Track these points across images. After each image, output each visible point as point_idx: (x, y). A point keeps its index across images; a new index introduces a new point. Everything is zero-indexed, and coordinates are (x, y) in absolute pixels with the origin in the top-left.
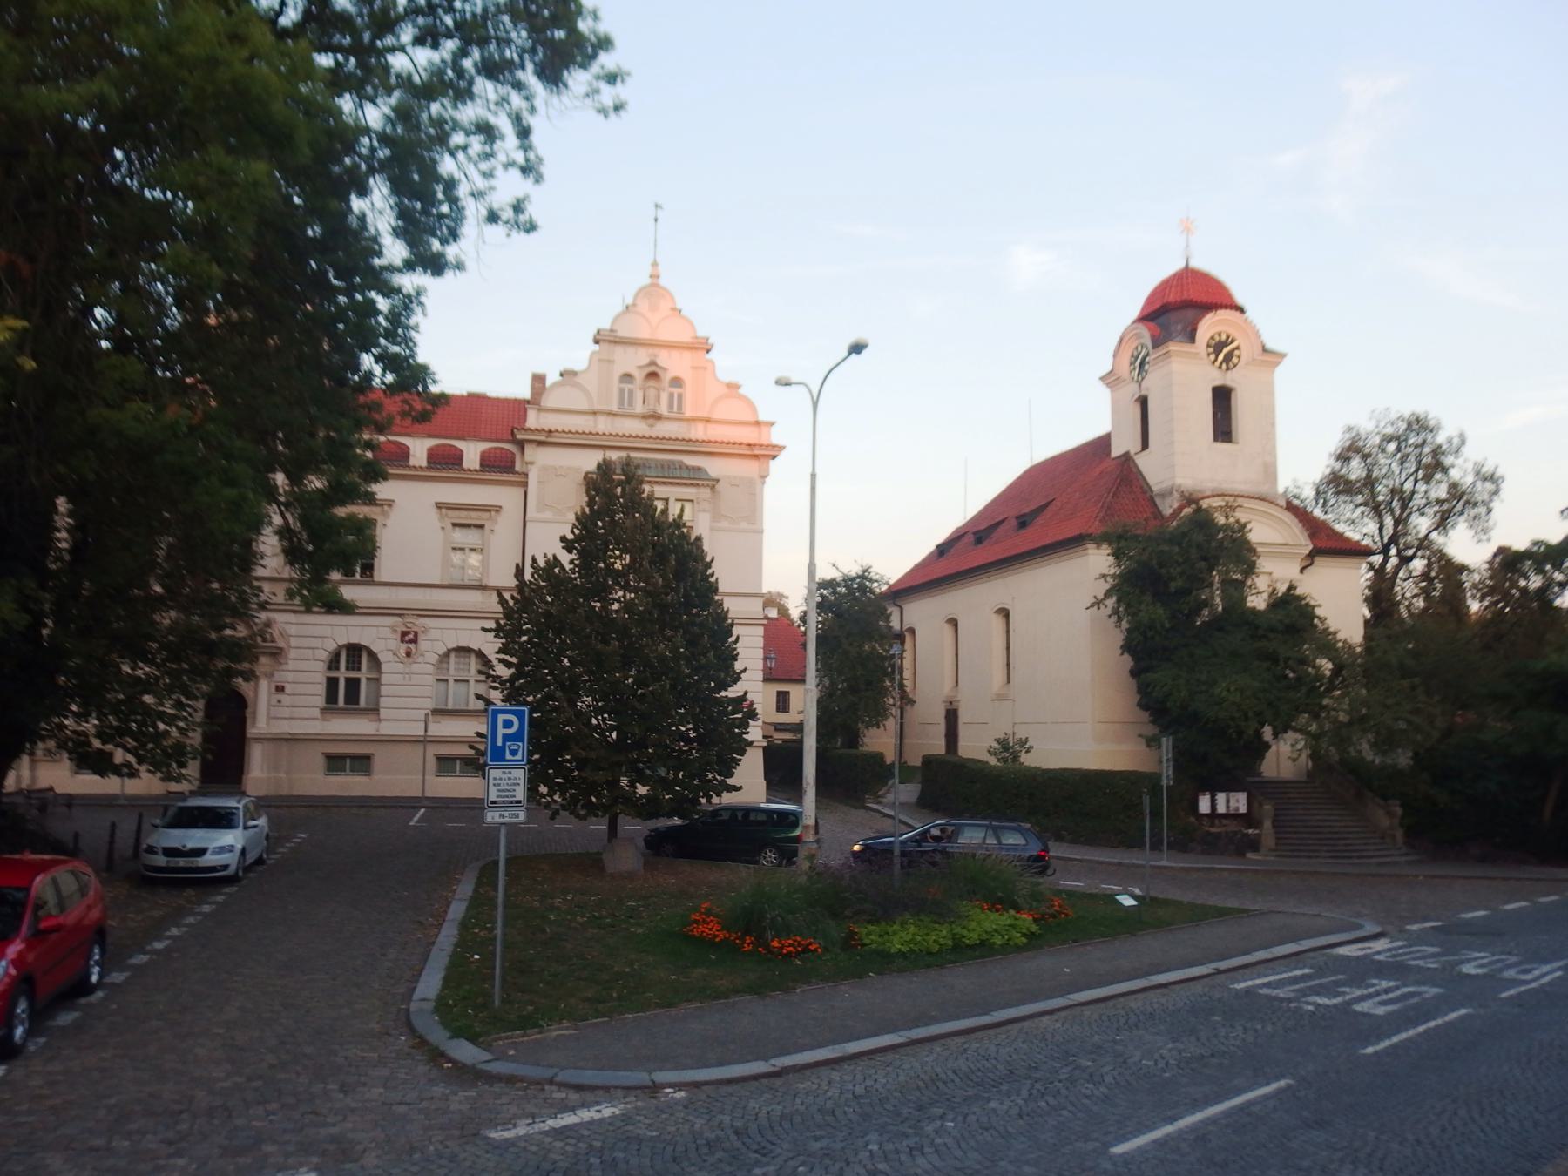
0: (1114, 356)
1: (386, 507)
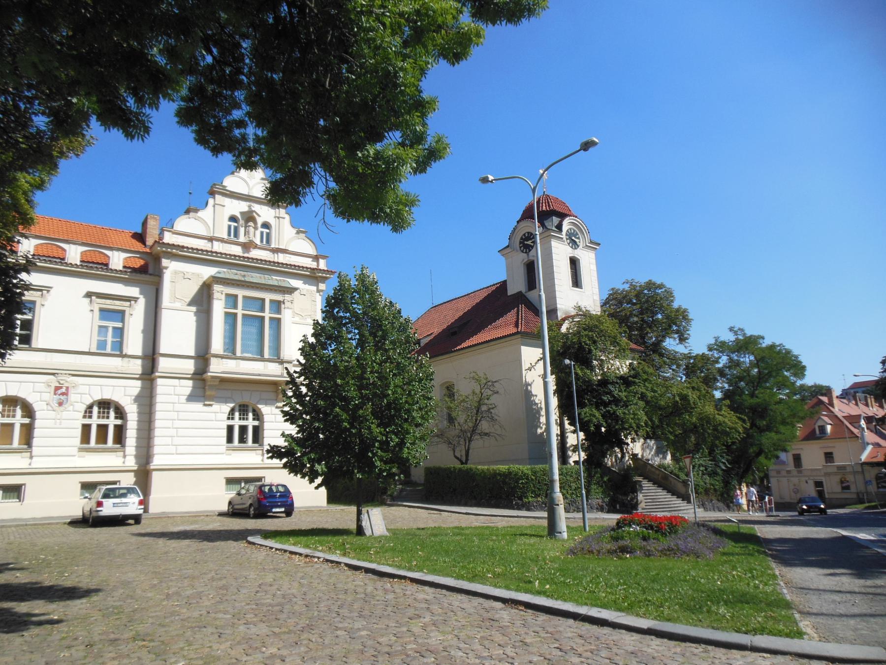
0: (518, 222)
1: (45, 292)
